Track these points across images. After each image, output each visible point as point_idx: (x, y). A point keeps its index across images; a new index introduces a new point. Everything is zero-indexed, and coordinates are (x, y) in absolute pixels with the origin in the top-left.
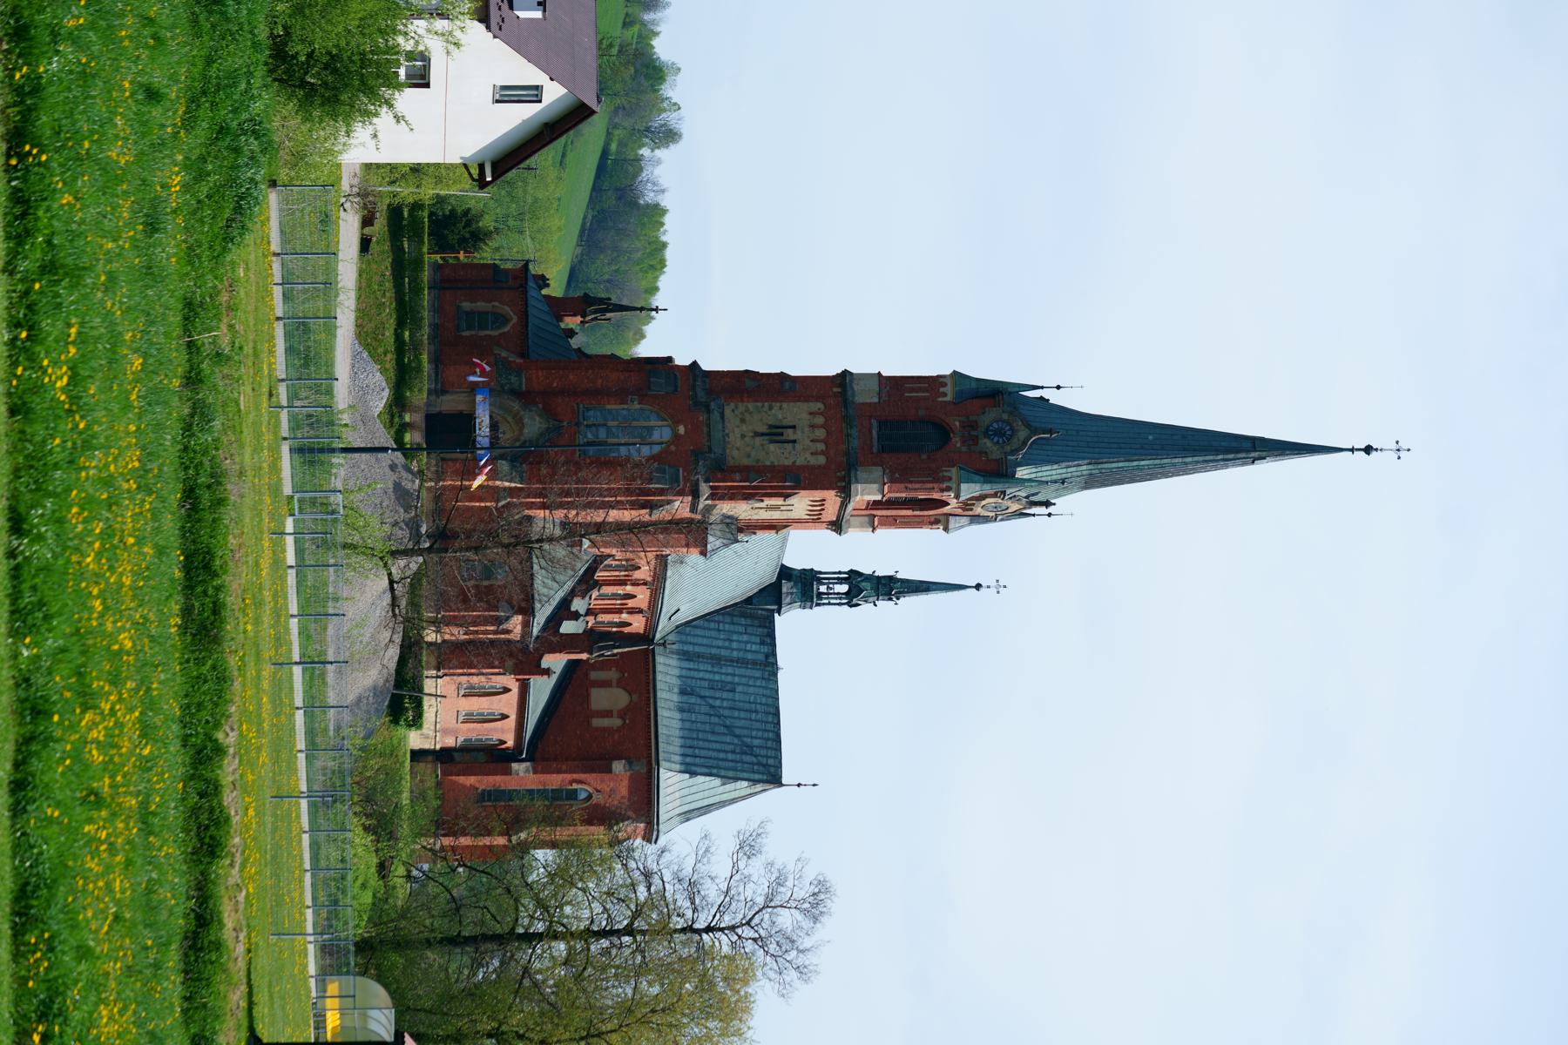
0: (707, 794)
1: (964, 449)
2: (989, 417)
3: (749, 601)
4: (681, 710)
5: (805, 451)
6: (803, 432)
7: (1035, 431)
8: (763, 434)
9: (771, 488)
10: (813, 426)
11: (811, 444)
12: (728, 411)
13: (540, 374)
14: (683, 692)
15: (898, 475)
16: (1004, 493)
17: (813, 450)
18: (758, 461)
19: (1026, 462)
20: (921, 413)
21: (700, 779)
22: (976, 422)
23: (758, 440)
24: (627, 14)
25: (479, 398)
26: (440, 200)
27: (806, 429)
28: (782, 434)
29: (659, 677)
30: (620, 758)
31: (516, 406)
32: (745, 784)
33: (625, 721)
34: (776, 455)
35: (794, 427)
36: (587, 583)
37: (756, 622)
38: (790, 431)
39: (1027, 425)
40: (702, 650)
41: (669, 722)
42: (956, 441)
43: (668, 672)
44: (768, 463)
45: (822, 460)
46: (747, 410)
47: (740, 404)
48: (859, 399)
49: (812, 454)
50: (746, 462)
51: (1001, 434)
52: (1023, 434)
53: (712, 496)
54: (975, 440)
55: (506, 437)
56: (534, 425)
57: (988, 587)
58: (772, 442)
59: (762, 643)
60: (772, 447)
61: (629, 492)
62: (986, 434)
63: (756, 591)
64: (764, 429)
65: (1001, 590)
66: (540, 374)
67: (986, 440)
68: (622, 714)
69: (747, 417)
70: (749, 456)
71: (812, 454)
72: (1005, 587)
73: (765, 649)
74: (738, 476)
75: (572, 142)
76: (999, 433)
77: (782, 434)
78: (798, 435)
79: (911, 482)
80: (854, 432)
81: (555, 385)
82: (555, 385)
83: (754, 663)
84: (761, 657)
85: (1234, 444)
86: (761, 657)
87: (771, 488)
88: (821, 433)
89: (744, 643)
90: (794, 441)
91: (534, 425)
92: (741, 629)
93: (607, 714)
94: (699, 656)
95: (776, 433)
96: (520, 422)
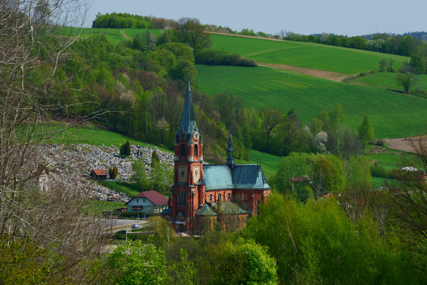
0: (260, 181)
2: (180, 138)
3: (231, 170)
4: (246, 184)
5: (185, 169)
7: (183, 130)
10: (182, 167)
12: (180, 181)
14: (243, 183)
15: (189, 154)
16: (192, 136)
19: (187, 132)
20: (180, 149)
21: (257, 181)
23: (184, 177)
24: (388, 71)
25: (176, 223)
26: (212, 211)
29: (240, 188)
30: (251, 196)
31: (177, 217)
34: (186, 174)
36: (210, 205)
39: (182, 131)
41: (246, 186)
42: (184, 143)
43: (240, 186)
45: (187, 166)
48: (178, 159)
51: (183, 136)
52: (183, 132)
53: (192, 185)
54: (184, 140)
55: (182, 218)
56: (180, 214)
61: (190, 199)
62: (183, 138)
63: (229, 169)
68: (245, 195)
75: (425, 95)
76: (183, 136)
80: (183, 160)
84: (240, 168)
86: (240, 168)
89: (238, 171)
91: (180, 214)
93: (245, 197)
94: (238, 180)
95: (183, 174)
96: (180, 216)
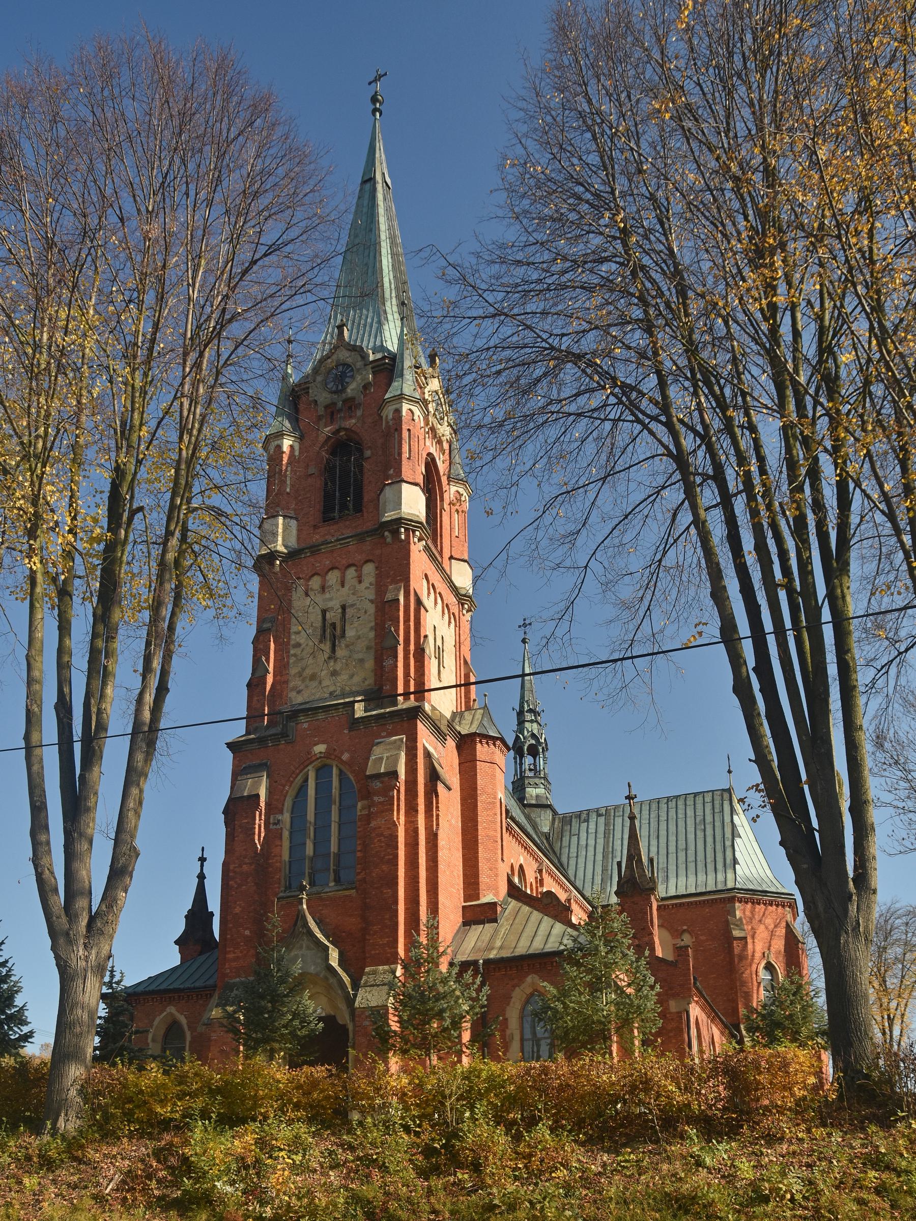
1: (444, 968)
6: (331, 599)
8: (333, 650)
9: (407, 620)
11: (347, 587)
13: (231, 956)
17: (355, 582)
18: (368, 648)
22: (326, 407)
23: (340, 653)
27: (327, 596)
28: (333, 625)
32: (735, 817)
33: (684, 931)
35: (324, 612)
37: (567, 828)
38: (328, 615)
40: (599, 869)
44: (372, 635)
45: (369, 569)
46: (300, 674)
47: (291, 685)
49: (360, 582)
50: (370, 664)
57: (525, 633)
58: (343, 635)
59: (587, 821)
60: (350, 633)
64: (326, 647)
65: (527, 622)
66: (231, 956)
67: (349, 390)
69: (308, 672)
70: (362, 661)
71: (360, 582)
72: (525, 620)
73: (593, 816)
74: (388, 663)
77: (333, 625)
78: (336, 604)
79: (400, 454)
81: (247, 933)
82: (247, 933)
83: (607, 824)
84: (602, 820)
85: (367, 196)
87: (407, 620)
88: (333, 577)
90: (344, 608)
92: (574, 839)
